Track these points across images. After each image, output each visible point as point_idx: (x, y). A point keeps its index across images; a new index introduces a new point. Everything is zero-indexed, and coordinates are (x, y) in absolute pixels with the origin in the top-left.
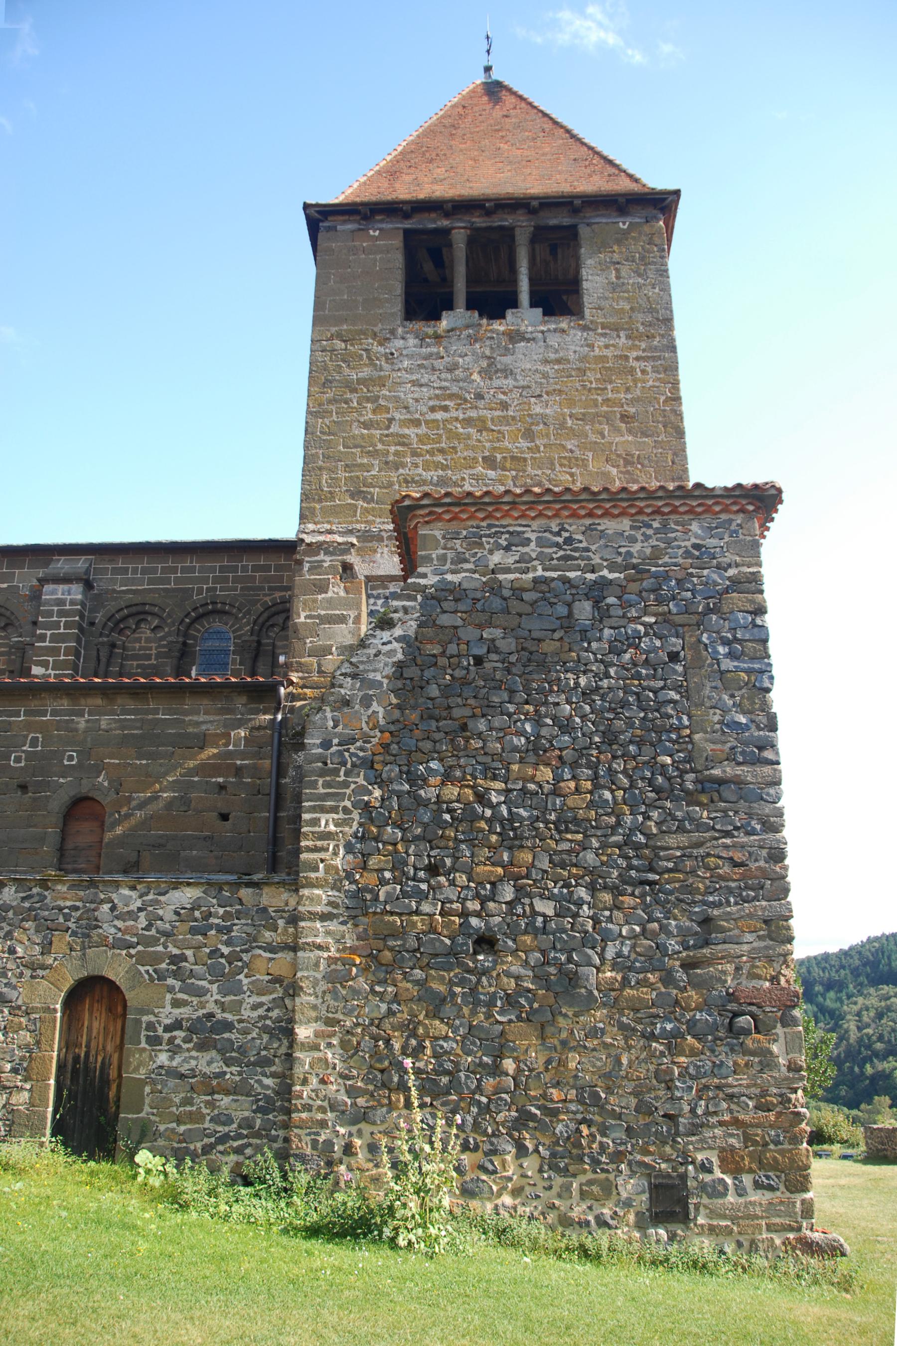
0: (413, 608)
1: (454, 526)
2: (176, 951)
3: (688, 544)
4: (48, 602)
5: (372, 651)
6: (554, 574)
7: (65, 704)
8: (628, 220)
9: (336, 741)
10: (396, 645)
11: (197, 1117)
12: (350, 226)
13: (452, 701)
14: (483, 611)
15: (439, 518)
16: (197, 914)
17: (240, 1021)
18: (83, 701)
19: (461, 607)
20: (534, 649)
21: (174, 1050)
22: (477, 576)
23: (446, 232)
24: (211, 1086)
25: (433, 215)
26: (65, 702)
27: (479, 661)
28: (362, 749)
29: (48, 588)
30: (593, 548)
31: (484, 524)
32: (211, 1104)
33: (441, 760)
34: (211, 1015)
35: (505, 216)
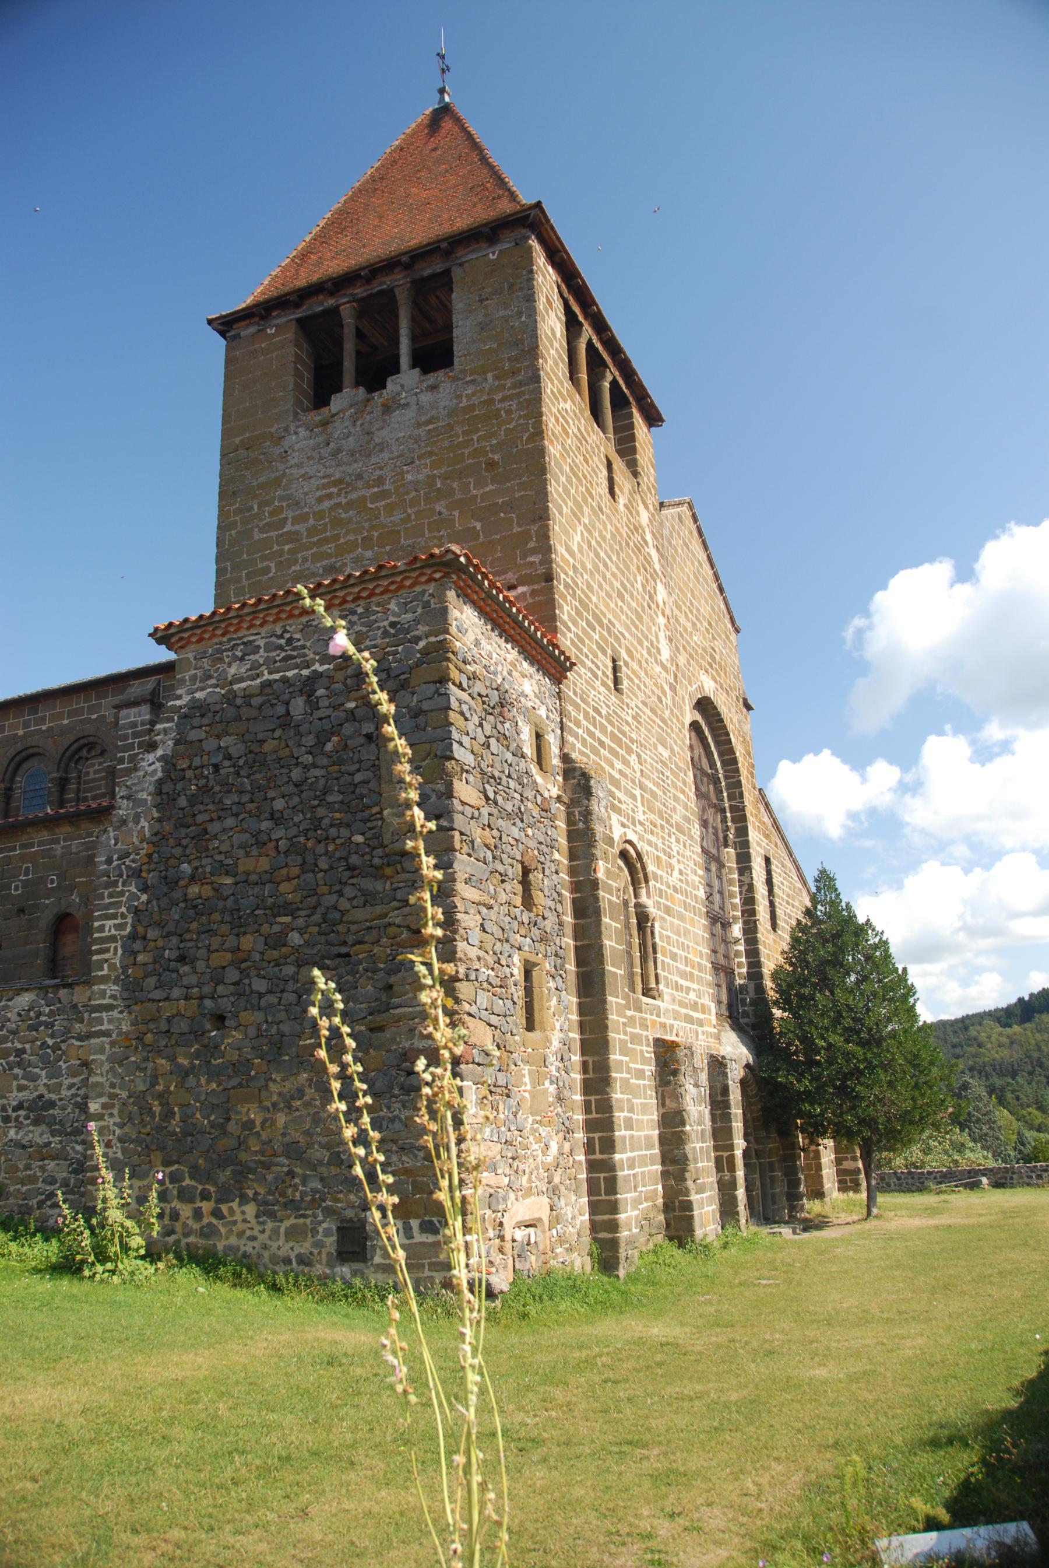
0: (171, 728)
1: (201, 647)
2: (19, 1046)
3: (386, 623)
4: (124, 727)
5: (142, 773)
6: (277, 676)
7: (45, 835)
8: (498, 248)
9: (116, 857)
10: (158, 764)
11: (33, 1179)
12: (252, 329)
13: (196, 809)
14: (221, 722)
15: (189, 642)
16: (32, 1014)
17: (61, 1099)
18: (57, 831)
19: (205, 721)
20: (258, 750)
21: (19, 1127)
22: (218, 690)
23: (335, 311)
24: (43, 1153)
25: (321, 297)
26: (45, 833)
27: (216, 767)
28: (133, 861)
29: (124, 712)
30: (308, 644)
31: (225, 639)
32: (42, 1168)
33: (189, 863)
34: (41, 1096)
35: (384, 279)
